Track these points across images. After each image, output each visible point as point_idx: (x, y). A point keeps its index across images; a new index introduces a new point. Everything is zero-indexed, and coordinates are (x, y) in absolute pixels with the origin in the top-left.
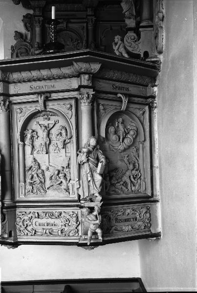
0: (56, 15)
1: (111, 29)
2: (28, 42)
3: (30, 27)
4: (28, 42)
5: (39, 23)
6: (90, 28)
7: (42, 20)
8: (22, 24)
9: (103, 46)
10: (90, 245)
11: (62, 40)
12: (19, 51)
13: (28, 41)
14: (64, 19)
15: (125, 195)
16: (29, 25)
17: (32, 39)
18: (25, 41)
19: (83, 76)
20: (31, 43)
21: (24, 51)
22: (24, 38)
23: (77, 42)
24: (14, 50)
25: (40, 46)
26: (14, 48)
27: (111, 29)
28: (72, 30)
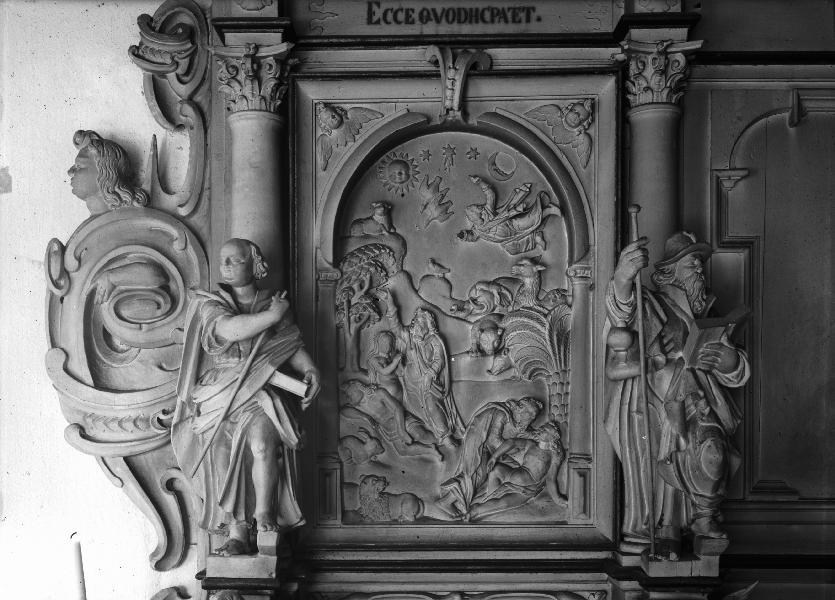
0: (733, 413)
1: (800, 116)
2: (173, 217)
3: (190, 100)
4: (173, 217)
5: (256, 76)
6: (649, 117)
7: (281, 60)
8: (135, 77)
9: (733, 245)
10: (193, 43)
11: (427, 195)
12: (103, 285)
13: (169, 202)
14: (441, 42)
15: (245, 12)
16: (184, 90)
17: (201, 191)
18: (150, 204)
19: (531, 414)
20: (197, 221)
21: (144, 279)
22: (146, 172)
23: (535, 217)
24: (64, 272)
25: (259, 268)
26: (71, 262)
27: (800, 116)
28: (501, 129)
